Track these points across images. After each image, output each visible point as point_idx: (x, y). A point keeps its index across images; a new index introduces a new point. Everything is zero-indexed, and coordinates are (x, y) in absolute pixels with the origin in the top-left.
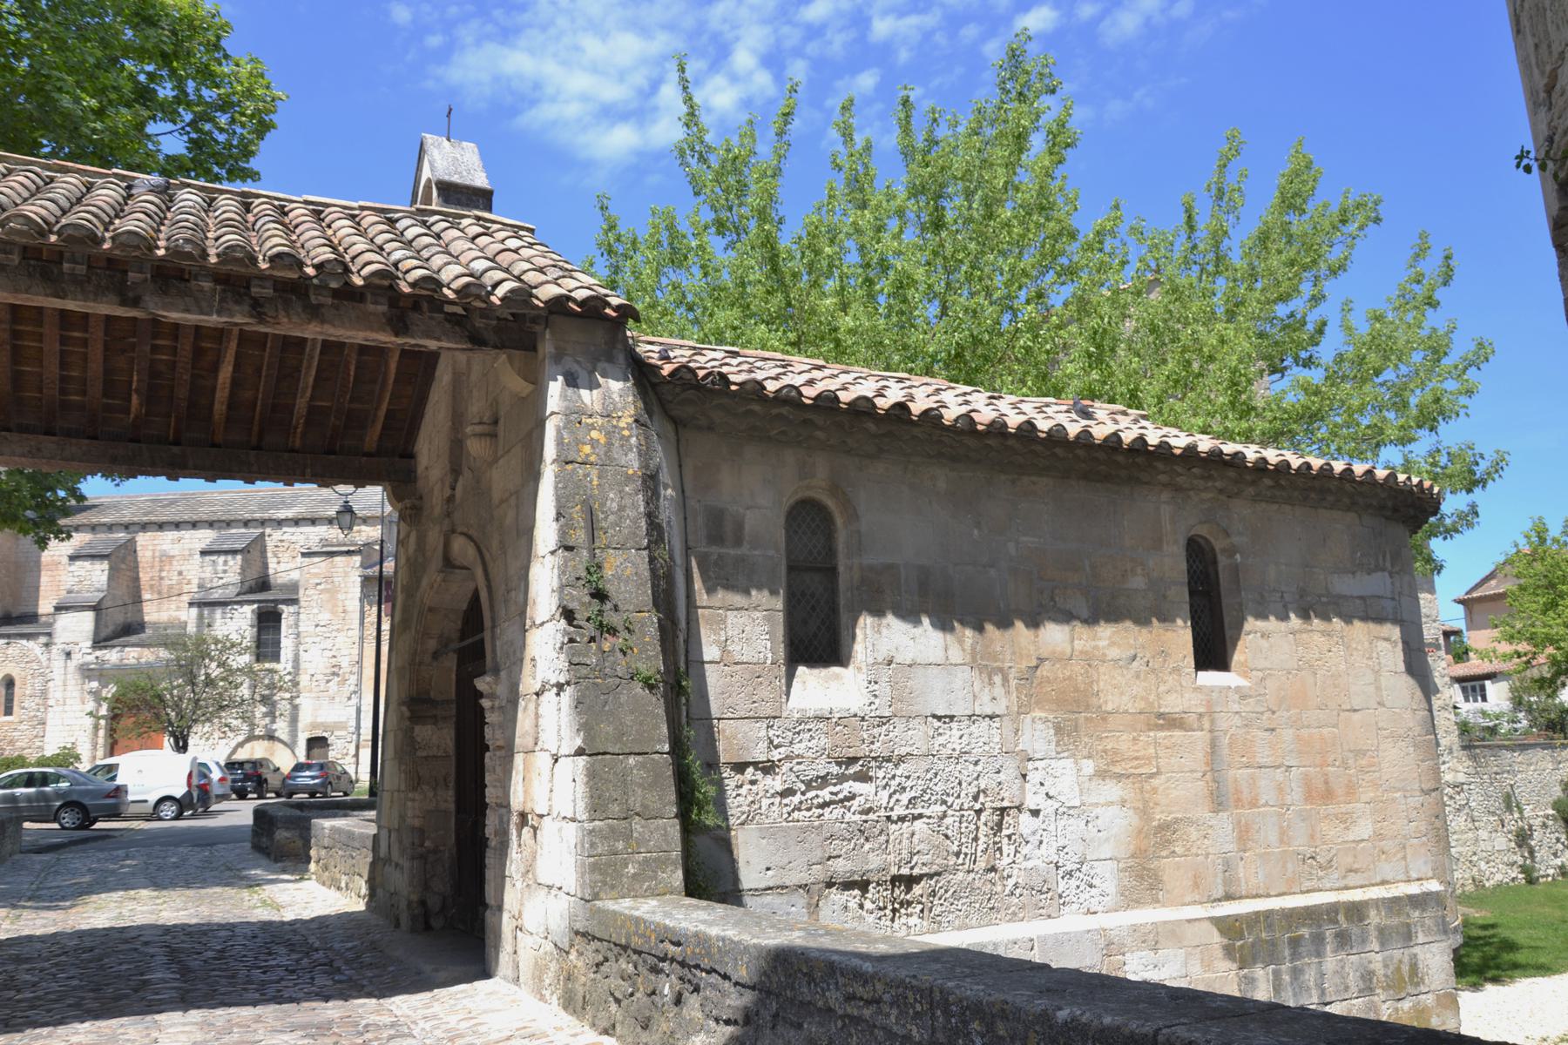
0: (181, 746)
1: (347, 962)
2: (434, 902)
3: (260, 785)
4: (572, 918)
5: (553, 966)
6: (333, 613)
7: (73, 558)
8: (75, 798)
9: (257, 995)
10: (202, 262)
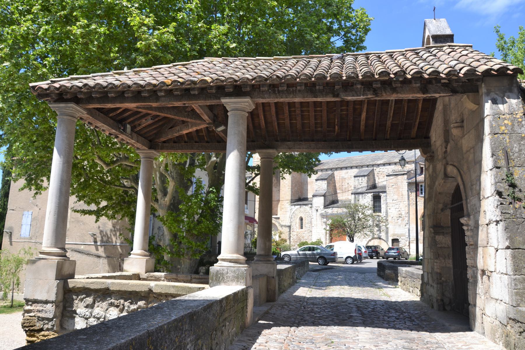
0: (352, 240)
1: (416, 318)
2: (446, 301)
3: (378, 255)
4: (508, 313)
5: (500, 330)
6: (398, 196)
7: (317, 180)
8: (322, 255)
9: (387, 325)
10: (357, 79)
